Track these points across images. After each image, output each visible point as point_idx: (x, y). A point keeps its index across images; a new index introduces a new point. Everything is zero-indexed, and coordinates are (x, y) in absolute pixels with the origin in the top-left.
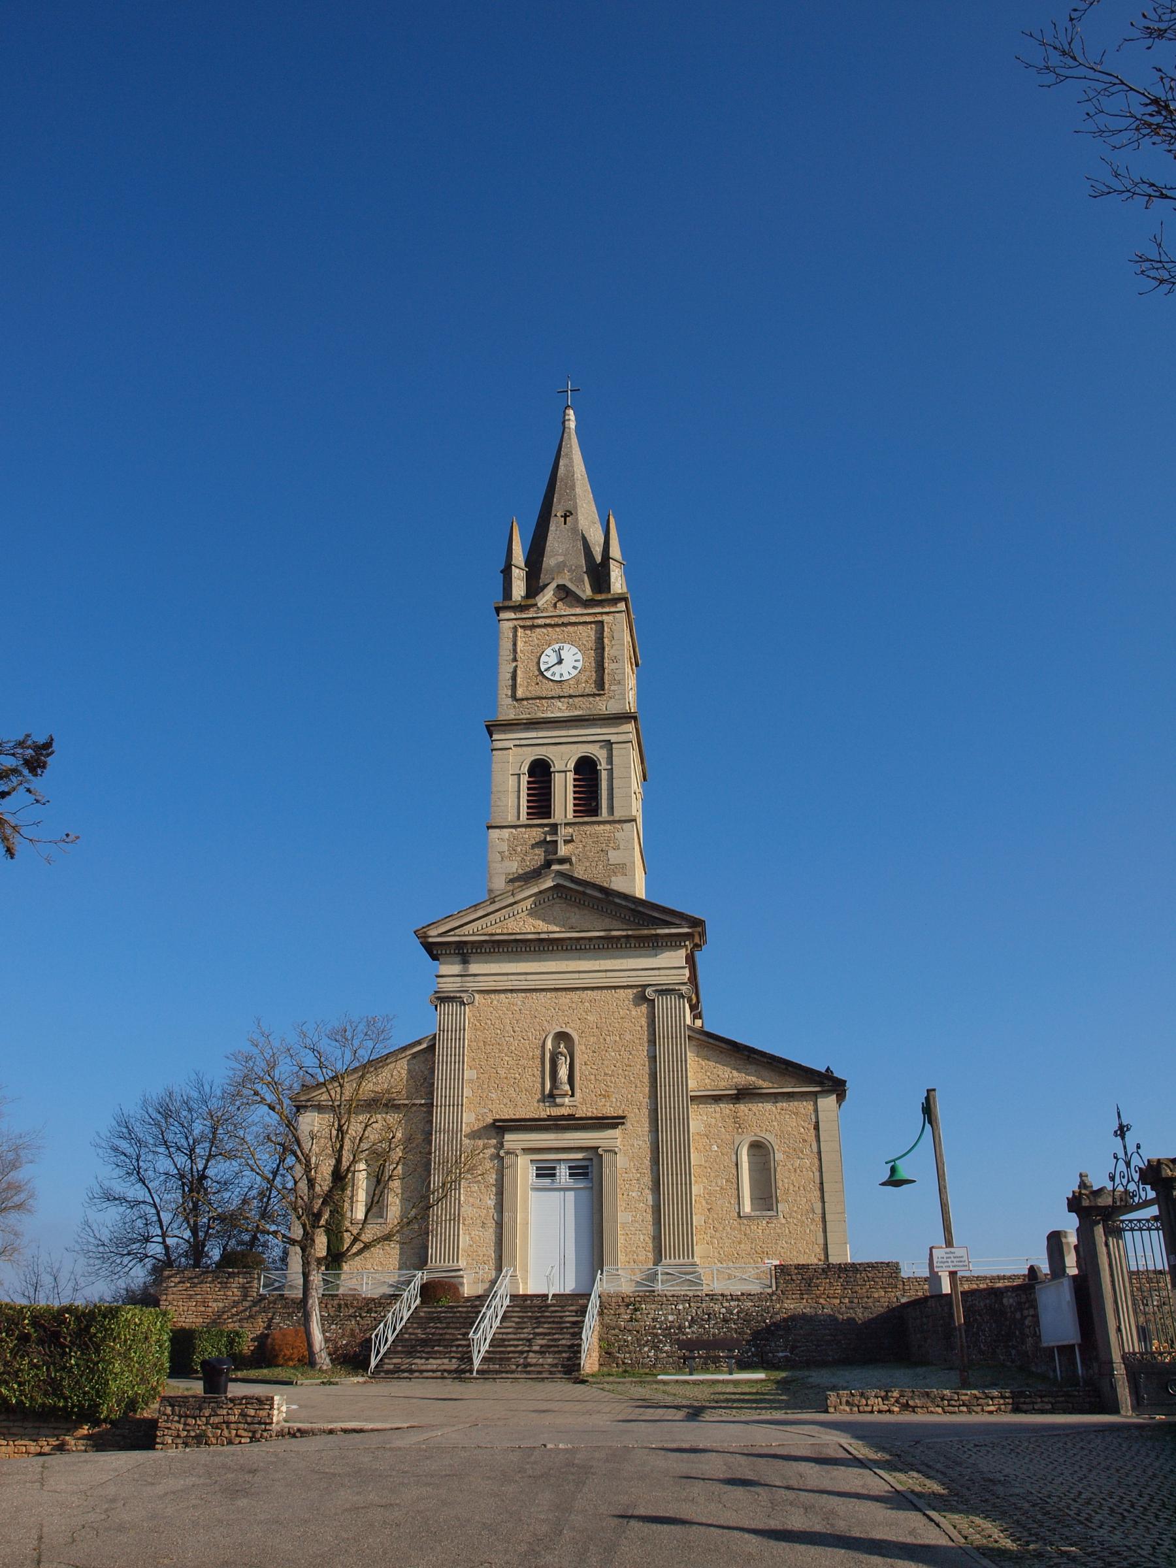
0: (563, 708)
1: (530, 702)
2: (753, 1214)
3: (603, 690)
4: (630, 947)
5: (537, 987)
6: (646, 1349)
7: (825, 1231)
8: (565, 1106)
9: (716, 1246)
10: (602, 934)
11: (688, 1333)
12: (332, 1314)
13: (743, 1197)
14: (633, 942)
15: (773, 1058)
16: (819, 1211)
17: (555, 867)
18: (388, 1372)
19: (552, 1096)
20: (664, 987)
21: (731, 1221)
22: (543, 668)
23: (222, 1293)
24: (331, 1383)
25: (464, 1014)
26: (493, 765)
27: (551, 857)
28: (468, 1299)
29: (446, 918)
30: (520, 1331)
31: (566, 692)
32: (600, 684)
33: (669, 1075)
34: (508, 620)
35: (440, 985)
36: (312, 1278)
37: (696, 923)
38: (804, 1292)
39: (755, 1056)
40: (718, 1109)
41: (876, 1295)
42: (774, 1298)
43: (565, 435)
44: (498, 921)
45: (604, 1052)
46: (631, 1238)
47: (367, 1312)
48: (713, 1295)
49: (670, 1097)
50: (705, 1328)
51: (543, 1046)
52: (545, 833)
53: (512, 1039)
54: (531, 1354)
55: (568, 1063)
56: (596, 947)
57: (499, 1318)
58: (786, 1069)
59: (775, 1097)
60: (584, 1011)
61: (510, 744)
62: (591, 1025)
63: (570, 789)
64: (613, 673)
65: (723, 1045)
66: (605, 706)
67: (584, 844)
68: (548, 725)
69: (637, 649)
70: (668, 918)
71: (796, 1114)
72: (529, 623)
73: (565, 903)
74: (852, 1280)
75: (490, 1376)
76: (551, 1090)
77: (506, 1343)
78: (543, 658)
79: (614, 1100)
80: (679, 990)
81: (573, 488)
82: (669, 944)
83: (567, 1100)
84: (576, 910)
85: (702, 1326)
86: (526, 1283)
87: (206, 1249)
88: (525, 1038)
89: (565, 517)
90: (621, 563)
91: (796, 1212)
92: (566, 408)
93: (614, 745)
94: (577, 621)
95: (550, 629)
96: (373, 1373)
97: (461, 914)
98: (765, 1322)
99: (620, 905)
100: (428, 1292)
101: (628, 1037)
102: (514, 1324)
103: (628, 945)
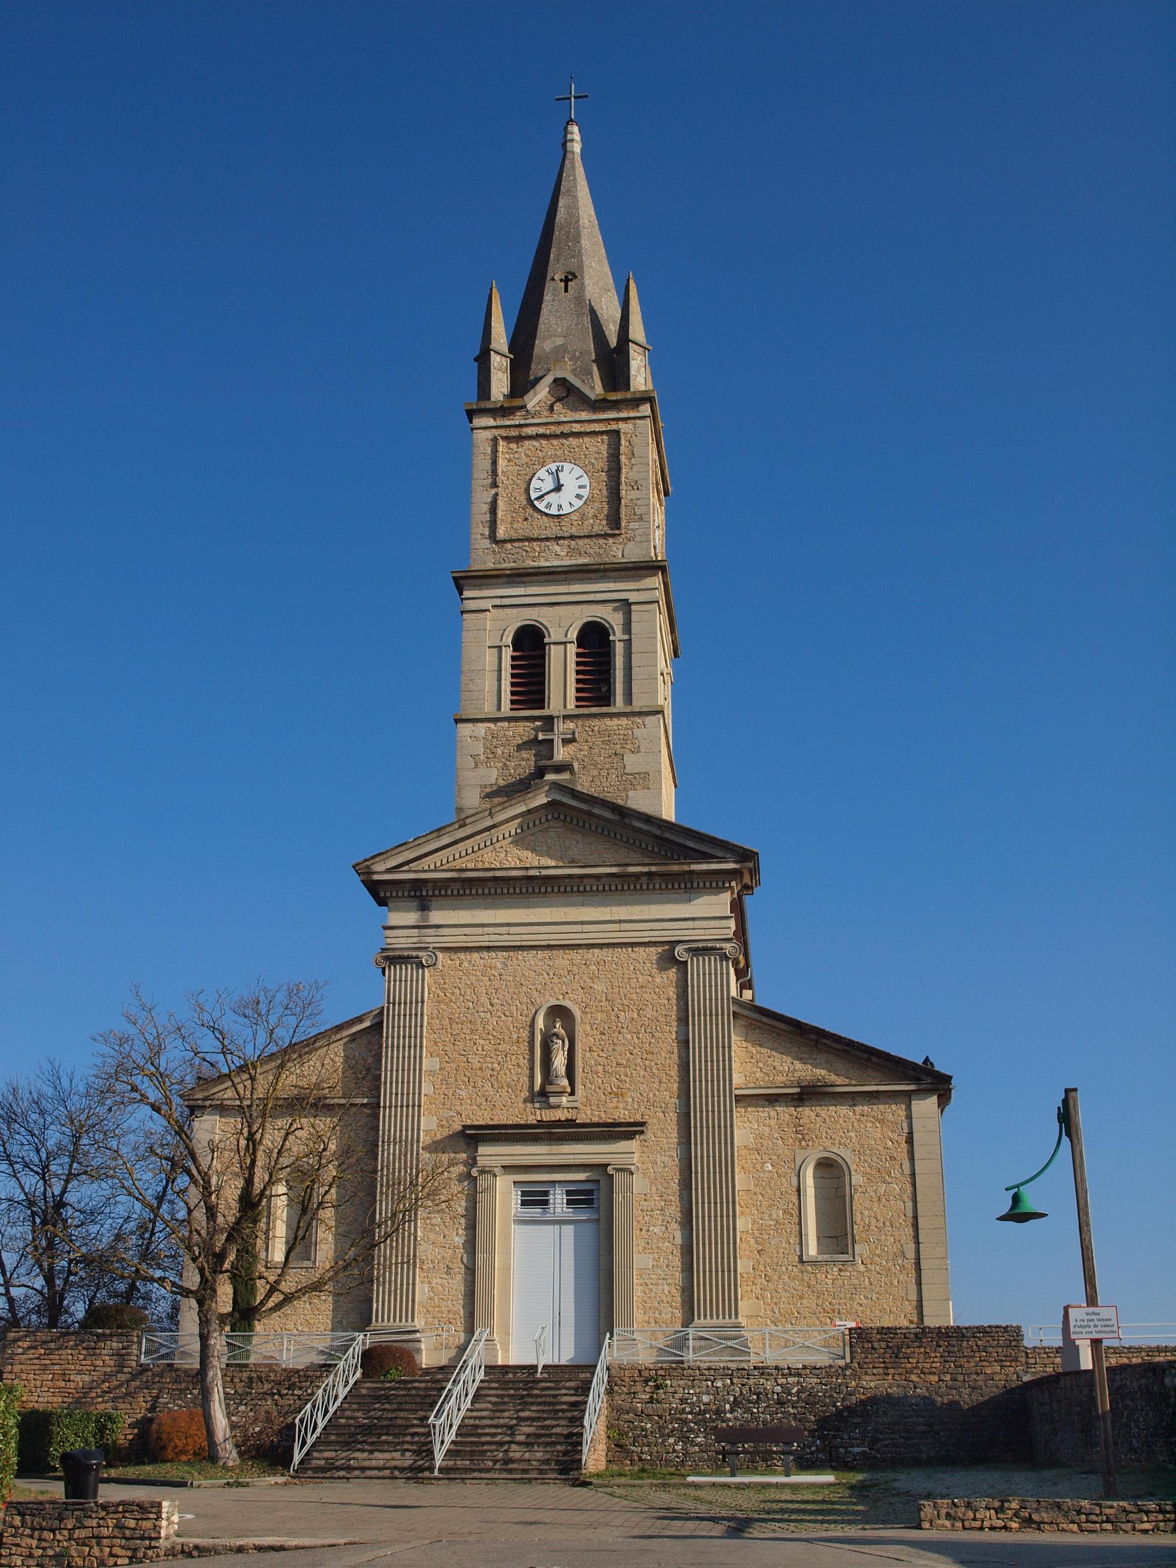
0: (562, 554)
1: (516, 544)
2: (820, 1258)
3: (619, 529)
4: (654, 889)
5: (524, 943)
6: (671, 1440)
7: (919, 1283)
8: (563, 1108)
9: (769, 1301)
10: (614, 870)
11: (729, 1420)
12: (240, 1391)
13: (807, 1235)
14: (657, 880)
16: (911, 1254)
17: (550, 777)
18: (316, 1469)
19: (544, 1094)
20: (700, 945)
21: (790, 1268)
22: (533, 495)
23: (89, 1362)
24: (239, 1485)
25: (423, 980)
26: (464, 634)
28: (427, 1372)
29: (398, 846)
30: (498, 1414)
31: (568, 530)
32: (614, 520)
33: (706, 1066)
34: (485, 428)
35: (389, 941)
36: (212, 1342)
37: (747, 856)
38: (890, 1366)
39: (826, 1041)
40: (773, 1113)
41: (989, 1371)
42: (848, 1372)
43: (567, 162)
44: (470, 851)
47: (289, 1389)
48: (763, 1368)
50: (752, 1414)
51: (532, 1025)
52: (536, 730)
54: (513, 1447)
55: (566, 1048)
56: (607, 888)
57: (470, 1397)
58: (869, 1059)
59: (852, 1098)
61: (487, 604)
62: (598, 997)
63: (572, 667)
64: (633, 505)
65: (782, 1026)
68: (542, 578)
69: (667, 471)
71: (882, 1122)
72: (514, 433)
74: (956, 1349)
76: (543, 1086)
78: (535, 483)
79: (630, 1100)
80: (722, 949)
81: (577, 239)
82: (708, 885)
84: (579, 836)
85: (748, 1410)
86: (507, 1350)
88: (507, 1013)
89: (566, 281)
90: (645, 348)
92: (568, 123)
93: (633, 607)
95: (544, 442)
96: (296, 1471)
97: (419, 842)
98: (835, 1406)
99: (639, 830)
100: (372, 1360)
101: (649, 1013)
102: (490, 1406)
103: (651, 886)
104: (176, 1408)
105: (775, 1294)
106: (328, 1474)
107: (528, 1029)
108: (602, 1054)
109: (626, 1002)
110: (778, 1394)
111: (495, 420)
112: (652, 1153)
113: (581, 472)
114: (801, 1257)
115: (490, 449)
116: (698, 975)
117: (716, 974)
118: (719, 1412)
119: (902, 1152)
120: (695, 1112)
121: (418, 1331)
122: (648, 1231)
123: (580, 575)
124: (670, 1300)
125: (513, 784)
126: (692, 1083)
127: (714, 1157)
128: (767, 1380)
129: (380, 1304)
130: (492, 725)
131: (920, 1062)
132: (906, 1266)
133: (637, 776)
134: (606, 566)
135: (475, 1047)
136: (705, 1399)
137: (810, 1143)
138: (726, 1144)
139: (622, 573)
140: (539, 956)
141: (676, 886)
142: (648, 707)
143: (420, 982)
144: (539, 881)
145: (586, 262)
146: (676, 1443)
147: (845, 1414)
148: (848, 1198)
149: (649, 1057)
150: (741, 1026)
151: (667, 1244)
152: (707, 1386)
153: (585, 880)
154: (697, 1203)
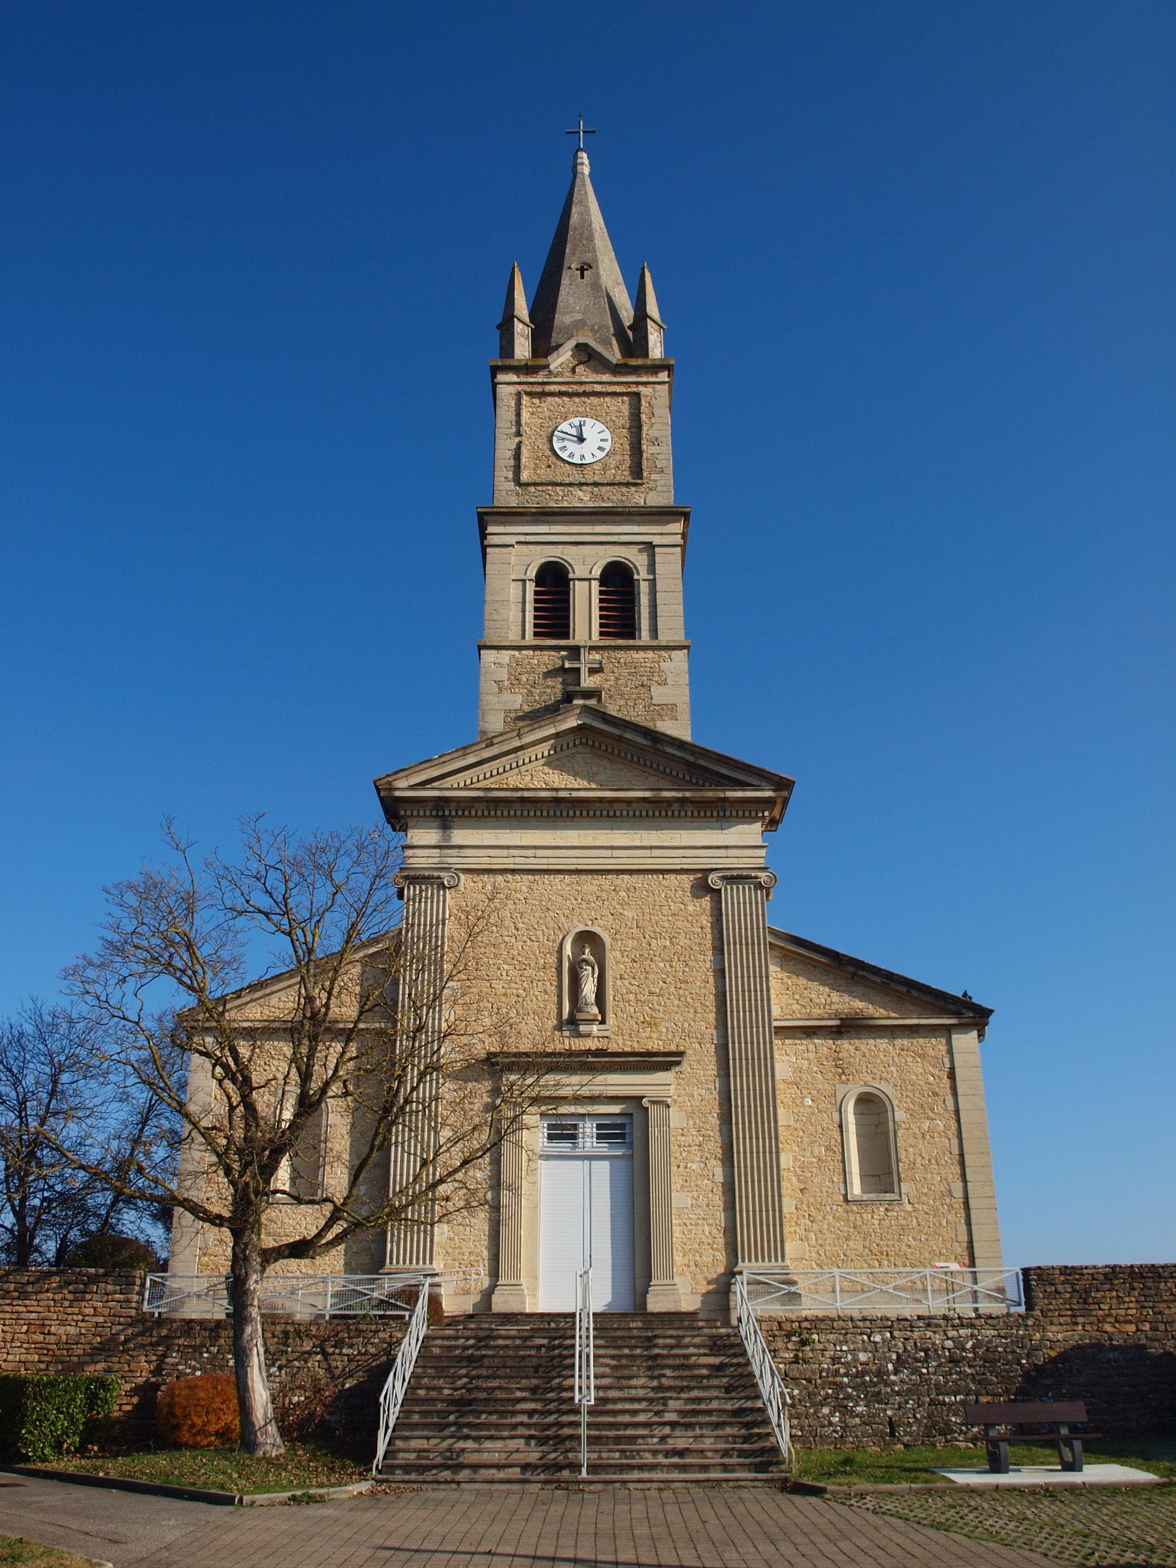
0: (585, 498)
1: (540, 488)
2: (865, 1197)
3: (641, 479)
5: (551, 867)
6: (826, 1410)
7: (969, 1223)
8: (594, 1037)
9: (814, 1242)
10: (647, 794)
11: (894, 1383)
13: (851, 1173)
14: (689, 808)
15: (890, 977)
16: (959, 1194)
17: (578, 702)
18: (407, 1468)
19: (573, 1022)
20: (735, 873)
23: (76, 1310)
24: (311, 1500)
25: (444, 902)
29: (421, 763)
30: (624, 1382)
31: (590, 478)
32: (637, 470)
33: (744, 996)
37: (783, 785)
38: (1078, 1313)
39: (865, 973)
42: (1030, 1322)
44: (495, 773)
45: (649, 962)
46: (691, 1231)
47: (335, 1346)
48: (930, 1318)
49: (745, 1028)
50: (921, 1374)
51: (560, 950)
52: (563, 659)
55: (596, 975)
56: (637, 813)
59: (892, 1031)
62: (629, 924)
66: (638, 498)
68: (567, 518)
70: (741, 777)
71: (923, 1056)
72: (538, 389)
73: (590, 753)
74: (1153, 1292)
75: (615, 1477)
76: (571, 1014)
77: (610, 1407)
79: (664, 1030)
80: (756, 878)
81: (591, 238)
82: (741, 813)
83: (595, 1028)
84: (606, 763)
85: (915, 1371)
87: (36, 1241)
88: (533, 938)
89: (582, 270)
90: (661, 327)
91: (926, 1195)
92: (577, 151)
94: (604, 390)
95: (566, 399)
96: (380, 1472)
97: (444, 759)
98: (1019, 1364)
101: (683, 941)
102: (608, 1370)
103: (683, 813)
104: (188, 1371)
105: (820, 1236)
106: (428, 1476)
107: (556, 955)
109: (657, 930)
110: (949, 1350)
111: (518, 377)
113: (603, 427)
114: (845, 1196)
115: (513, 402)
117: (751, 903)
118: (881, 1373)
119: (944, 1087)
120: (733, 1043)
121: (437, 1275)
122: (686, 1167)
123: (605, 517)
124: (711, 1242)
125: (538, 711)
126: (729, 1013)
127: (755, 1090)
128: (935, 1332)
130: (516, 653)
131: (960, 995)
132: (955, 1205)
133: (665, 707)
134: (631, 510)
135: (499, 972)
136: (863, 1357)
137: (851, 1077)
138: (766, 1076)
139: (645, 518)
140: (567, 881)
141: (709, 814)
142: (675, 641)
143: (441, 904)
144: (568, 805)
145: (600, 257)
146: (832, 1414)
147: (1033, 1373)
148: (891, 1135)
149: (682, 985)
150: (776, 957)
151: (706, 1181)
152: (863, 1341)
154: (738, 1138)
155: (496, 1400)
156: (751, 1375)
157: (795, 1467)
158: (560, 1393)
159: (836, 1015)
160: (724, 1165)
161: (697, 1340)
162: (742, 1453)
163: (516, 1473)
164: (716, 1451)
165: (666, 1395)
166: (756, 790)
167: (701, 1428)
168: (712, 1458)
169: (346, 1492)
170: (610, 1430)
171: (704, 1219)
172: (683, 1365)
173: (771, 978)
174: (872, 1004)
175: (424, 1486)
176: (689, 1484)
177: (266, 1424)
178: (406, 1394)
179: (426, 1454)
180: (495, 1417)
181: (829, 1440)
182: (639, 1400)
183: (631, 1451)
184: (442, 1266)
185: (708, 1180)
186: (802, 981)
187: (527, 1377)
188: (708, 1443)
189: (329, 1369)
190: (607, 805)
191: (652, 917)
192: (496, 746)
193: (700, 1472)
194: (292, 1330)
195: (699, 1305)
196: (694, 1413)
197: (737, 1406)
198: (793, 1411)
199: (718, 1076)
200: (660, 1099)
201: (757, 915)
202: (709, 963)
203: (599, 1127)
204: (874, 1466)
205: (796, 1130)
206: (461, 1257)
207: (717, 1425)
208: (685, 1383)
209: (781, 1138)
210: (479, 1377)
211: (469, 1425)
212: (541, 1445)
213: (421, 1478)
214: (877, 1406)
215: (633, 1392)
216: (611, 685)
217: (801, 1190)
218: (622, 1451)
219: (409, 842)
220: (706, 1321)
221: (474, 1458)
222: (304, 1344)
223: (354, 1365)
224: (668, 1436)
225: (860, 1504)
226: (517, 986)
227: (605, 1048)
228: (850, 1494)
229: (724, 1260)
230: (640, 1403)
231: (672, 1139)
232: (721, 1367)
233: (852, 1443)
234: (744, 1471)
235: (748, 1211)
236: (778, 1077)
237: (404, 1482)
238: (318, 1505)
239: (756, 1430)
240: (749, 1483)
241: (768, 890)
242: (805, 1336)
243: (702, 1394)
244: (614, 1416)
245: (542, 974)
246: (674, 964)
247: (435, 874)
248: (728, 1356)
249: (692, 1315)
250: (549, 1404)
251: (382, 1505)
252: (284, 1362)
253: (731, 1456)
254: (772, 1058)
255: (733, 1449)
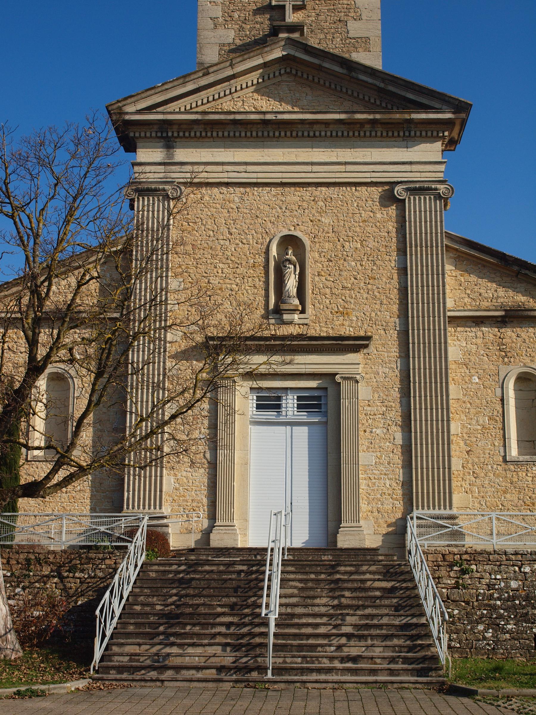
2: (521, 458)
4: (376, 136)
5: (259, 181)
6: (481, 627)
9: (477, 495)
10: (343, 116)
12: (17, 573)
13: (509, 438)
14: (379, 129)
17: (282, 35)
18: (120, 669)
19: (278, 311)
21: (495, 466)
24: (33, 694)
27: (276, 23)
28: (179, 553)
30: (309, 601)
33: (423, 290)
39: (527, 272)
40: (479, 334)
44: (211, 99)
46: (374, 484)
47: (69, 571)
49: (423, 317)
51: (267, 252)
53: (227, 243)
55: (297, 272)
56: (334, 134)
60: (318, 212)
62: (326, 229)
67: (318, 12)
76: (277, 305)
77: (296, 621)
79: (354, 319)
80: (436, 189)
82: (424, 134)
83: (296, 317)
86: (245, 535)
88: (244, 241)
97: (166, 87)
101: (371, 243)
102: (296, 591)
103: (373, 134)
106: (137, 676)
107: (263, 255)
108: (329, 278)
109: (350, 234)
112: (374, 365)
114: (504, 457)
116: (415, 212)
117: (431, 212)
120: (413, 330)
121: (165, 517)
122: (371, 432)
125: (248, 44)
126: (410, 305)
127: (430, 369)
129: (131, 493)
133: (359, 40)
137: (512, 360)
138: (440, 357)
140: (273, 193)
141: (396, 134)
146: (486, 630)
149: (371, 281)
150: (451, 258)
151: (388, 444)
152: (515, 572)
153: (315, 126)
154: (415, 409)
155: (199, 615)
156: (417, 597)
157: (452, 673)
158: (254, 609)
159: (502, 307)
160: (403, 431)
161: (373, 568)
162: (406, 660)
163: (212, 674)
164: (384, 658)
165: (344, 612)
166: (438, 113)
167: (372, 639)
168: (380, 664)
169: (64, 688)
170: (295, 640)
171: (385, 474)
172: (360, 588)
173: (446, 275)
174: (533, 298)
175: (133, 684)
176: (359, 685)
177: (6, 633)
178: (124, 608)
179: (137, 657)
180: (198, 628)
181: (483, 651)
182: (321, 616)
183: (312, 657)
184: (169, 510)
185: (390, 442)
186: (473, 278)
187: (227, 596)
188: (377, 652)
189: (65, 589)
190: (307, 126)
191: (346, 223)
192: (212, 75)
193: (370, 675)
194: (33, 557)
195: (380, 544)
196: (367, 627)
197: (404, 622)
198: (453, 628)
199: (400, 357)
200: (350, 376)
201: (436, 222)
202: (394, 262)
203: (299, 398)
204: (520, 674)
205: (464, 402)
206: (185, 503)
207: (386, 637)
208: (360, 603)
209: (452, 409)
210: (187, 596)
211: (175, 635)
212: (235, 651)
213: (130, 677)
214: (524, 624)
215: (316, 609)
216: (312, 21)
217: (468, 452)
218: (304, 657)
219: (138, 160)
220: (385, 555)
221: (178, 661)
222: (44, 570)
223: (85, 586)
224: (344, 645)
225: (506, 705)
226: (230, 282)
227: (305, 333)
228: (498, 696)
229: (402, 508)
230: (321, 618)
231: (360, 409)
232: (393, 590)
233: (502, 654)
234: (407, 675)
235: (422, 468)
236: (450, 359)
237: (116, 680)
238: (40, 699)
239: (420, 642)
240: (411, 685)
241: (446, 200)
242: (465, 566)
243: (375, 611)
244: (299, 629)
245: (252, 272)
246: (364, 263)
247: (161, 187)
248: (399, 582)
249: (374, 551)
250: (245, 618)
251: (94, 699)
252: (27, 584)
253: (397, 663)
254: (446, 342)
255: (399, 657)
